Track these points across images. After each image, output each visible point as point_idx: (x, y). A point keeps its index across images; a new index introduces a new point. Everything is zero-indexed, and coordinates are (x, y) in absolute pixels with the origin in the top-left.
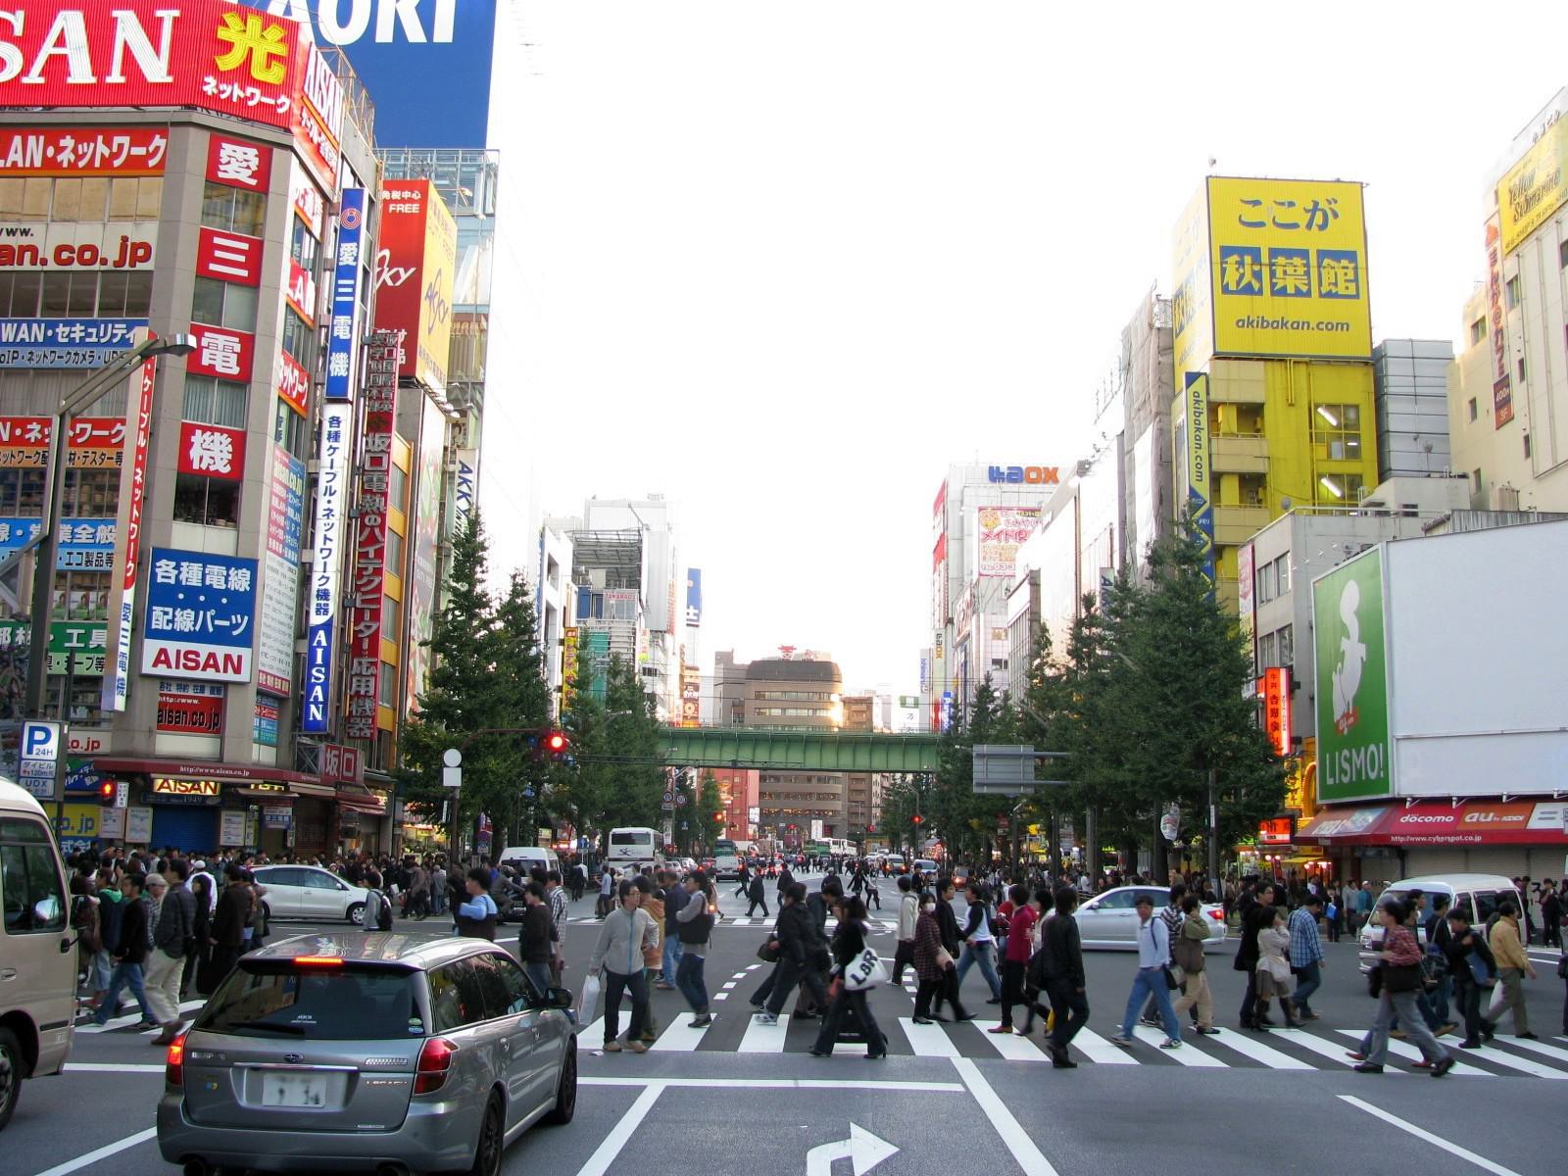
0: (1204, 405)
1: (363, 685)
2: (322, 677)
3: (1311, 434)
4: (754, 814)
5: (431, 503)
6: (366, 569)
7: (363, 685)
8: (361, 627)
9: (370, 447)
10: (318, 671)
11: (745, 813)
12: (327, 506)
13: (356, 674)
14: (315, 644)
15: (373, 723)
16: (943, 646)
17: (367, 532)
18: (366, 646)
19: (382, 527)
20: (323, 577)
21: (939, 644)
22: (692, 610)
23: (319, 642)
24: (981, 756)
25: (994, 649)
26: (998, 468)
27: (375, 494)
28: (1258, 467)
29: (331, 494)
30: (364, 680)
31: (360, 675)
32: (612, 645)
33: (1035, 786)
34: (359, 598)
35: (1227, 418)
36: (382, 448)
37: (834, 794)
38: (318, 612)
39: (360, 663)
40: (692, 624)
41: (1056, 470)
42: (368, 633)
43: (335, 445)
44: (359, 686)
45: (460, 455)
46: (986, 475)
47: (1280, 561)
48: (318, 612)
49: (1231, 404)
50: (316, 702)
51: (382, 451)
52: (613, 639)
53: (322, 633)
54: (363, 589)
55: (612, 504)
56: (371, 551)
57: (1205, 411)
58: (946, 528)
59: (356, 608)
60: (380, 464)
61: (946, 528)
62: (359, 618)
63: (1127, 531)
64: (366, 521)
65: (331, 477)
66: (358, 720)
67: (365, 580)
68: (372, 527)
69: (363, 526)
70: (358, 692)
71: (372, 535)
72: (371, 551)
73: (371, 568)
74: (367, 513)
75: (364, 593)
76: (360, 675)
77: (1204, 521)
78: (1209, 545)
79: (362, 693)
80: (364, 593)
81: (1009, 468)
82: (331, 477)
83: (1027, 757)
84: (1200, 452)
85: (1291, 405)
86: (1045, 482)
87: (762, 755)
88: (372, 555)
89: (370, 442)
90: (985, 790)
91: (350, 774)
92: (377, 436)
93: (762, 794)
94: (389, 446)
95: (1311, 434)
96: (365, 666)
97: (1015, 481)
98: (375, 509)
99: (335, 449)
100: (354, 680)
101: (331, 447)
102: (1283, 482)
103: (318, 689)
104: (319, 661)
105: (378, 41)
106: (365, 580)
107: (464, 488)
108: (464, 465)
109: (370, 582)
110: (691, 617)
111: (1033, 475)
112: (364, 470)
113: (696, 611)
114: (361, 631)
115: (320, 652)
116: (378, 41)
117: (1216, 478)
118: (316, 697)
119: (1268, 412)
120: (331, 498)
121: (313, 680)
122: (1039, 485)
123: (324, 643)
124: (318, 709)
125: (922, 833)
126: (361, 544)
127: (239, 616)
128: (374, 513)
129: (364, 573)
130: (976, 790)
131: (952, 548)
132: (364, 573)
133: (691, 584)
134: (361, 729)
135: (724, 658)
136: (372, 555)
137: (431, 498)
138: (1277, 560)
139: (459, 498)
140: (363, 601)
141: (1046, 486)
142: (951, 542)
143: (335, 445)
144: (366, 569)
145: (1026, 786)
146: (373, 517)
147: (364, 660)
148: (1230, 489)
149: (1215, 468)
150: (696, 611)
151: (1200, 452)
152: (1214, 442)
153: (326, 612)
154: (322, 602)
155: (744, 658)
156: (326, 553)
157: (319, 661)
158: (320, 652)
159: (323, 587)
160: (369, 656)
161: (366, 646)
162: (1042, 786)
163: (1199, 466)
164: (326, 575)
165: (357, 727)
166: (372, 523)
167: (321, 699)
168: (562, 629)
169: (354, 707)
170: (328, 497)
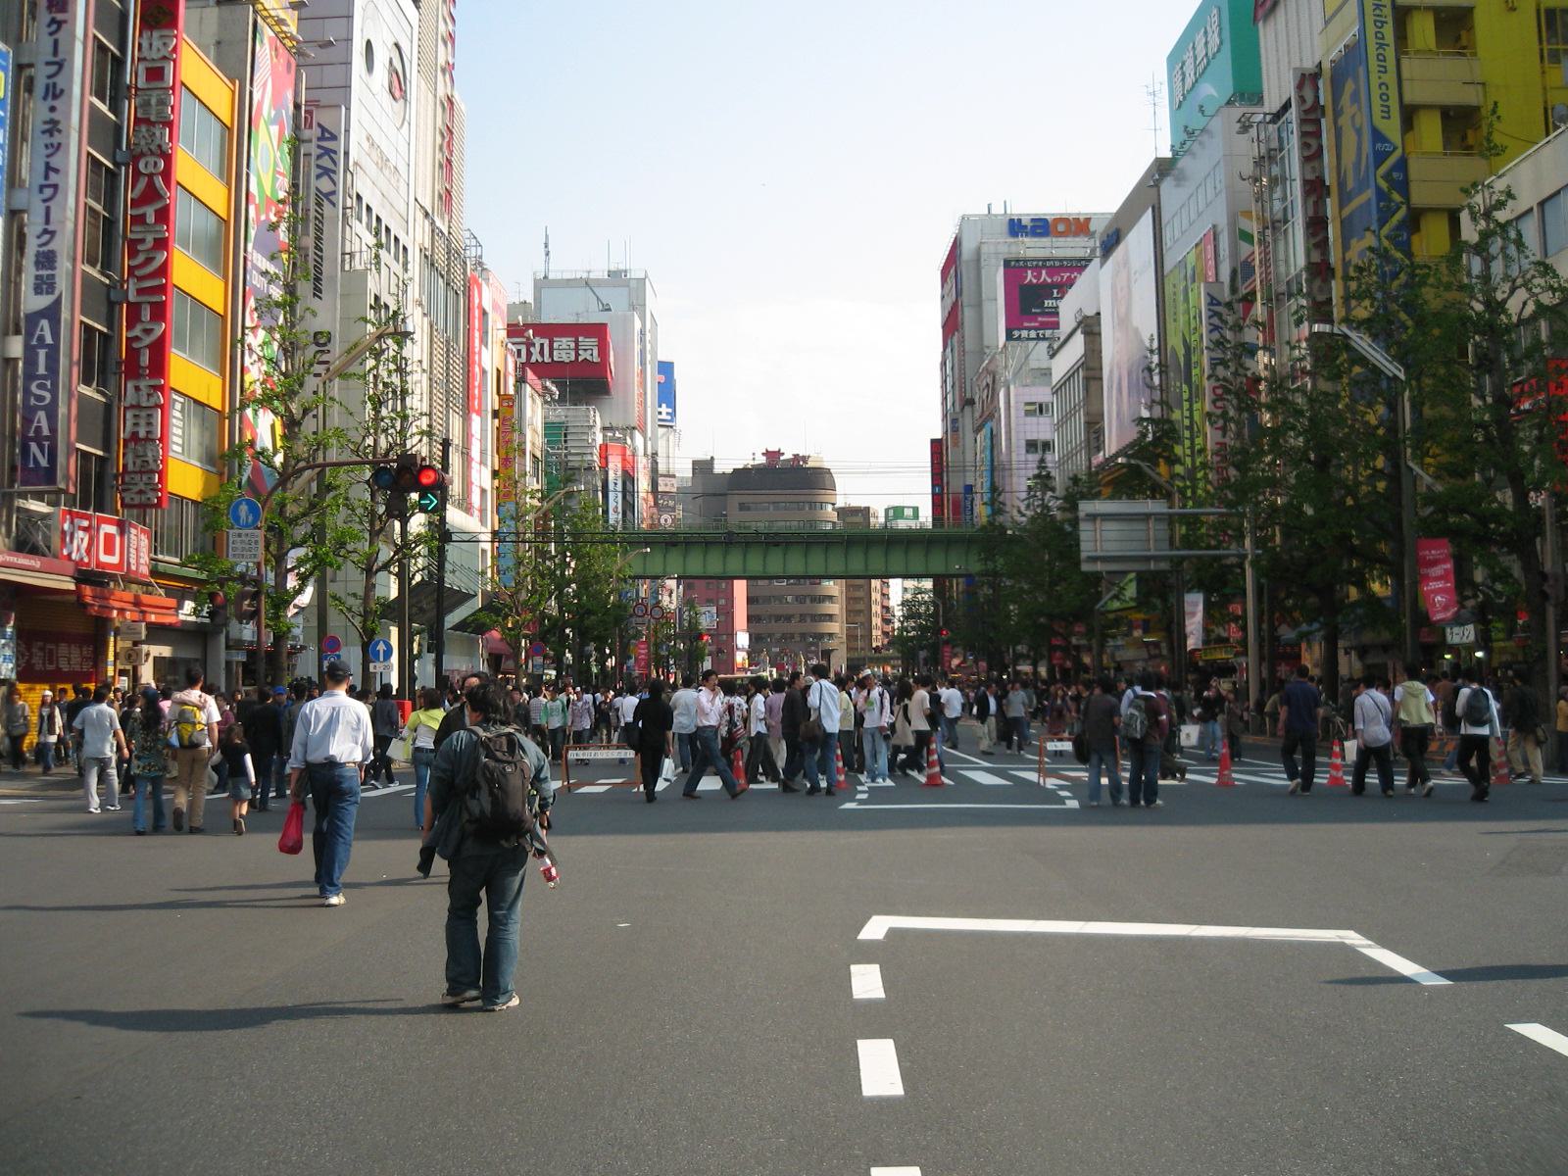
0: (1388, 11)
1: (142, 422)
2: (48, 396)
3: (1542, 50)
4: (742, 639)
5: (274, 180)
6: (142, 241)
7: (142, 422)
8: (137, 331)
9: (146, 53)
10: (41, 387)
11: (732, 635)
12: (48, 116)
13: (132, 407)
14: (34, 342)
15: (161, 480)
16: (960, 433)
17: (142, 183)
18: (145, 359)
19: (167, 175)
20: (45, 231)
21: (955, 430)
22: (664, 409)
23: (41, 338)
24: (1093, 517)
25: (1028, 427)
26: (1020, 220)
27: (153, 124)
28: (1469, 97)
29: (55, 97)
30: (143, 414)
31: (138, 406)
32: (569, 438)
33: (1171, 559)
34: (132, 288)
35: (1423, 30)
36: (164, 53)
37: (831, 616)
38: (38, 290)
39: (137, 389)
40: (668, 425)
41: (1088, 220)
42: (148, 340)
43: (60, 17)
44: (136, 424)
45: (321, 117)
46: (1005, 228)
47: (1547, 206)
48: (38, 290)
49: (1427, 8)
50: (38, 438)
51: (165, 58)
52: (571, 430)
53: (45, 323)
54: (137, 273)
55: (569, 283)
56: (150, 212)
57: (1390, 20)
58: (959, 293)
59: (129, 304)
60: (148, 70)
61: (959, 293)
62: (134, 318)
63: (995, 453)
64: (141, 166)
65: (54, 68)
66: (137, 477)
67: (141, 259)
68: (151, 176)
69: (137, 174)
70: (134, 436)
71: (151, 185)
72: (150, 212)
73: (150, 239)
74: (142, 155)
75: (141, 279)
76: (138, 406)
77: (1395, 175)
78: (1404, 210)
79: (142, 434)
80: (141, 279)
81: (1033, 220)
82: (54, 68)
83: (1158, 517)
84: (1385, 78)
85: (1513, 9)
86: (1076, 234)
87: (755, 564)
88: (151, 219)
89: (145, 44)
90: (1099, 567)
91: (114, 560)
92: (156, 34)
93: (749, 619)
94: (175, 50)
95: (1542, 50)
96: (144, 391)
97: (1041, 235)
98: (153, 147)
99: (60, 24)
100: (129, 415)
101: (53, 21)
102: (1515, 108)
103: (42, 415)
104: (42, 370)
105: (860, 1043)
106: (141, 259)
107: (326, 162)
108: (323, 129)
109: (149, 260)
110: (664, 416)
111: (1061, 228)
112: (137, 89)
113: (670, 410)
114: (137, 339)
115: (42, 353)
116: (860, 1043)
117: (1409, 115)
118: (38, 429)
119: (1480, 19)
120: (55, 103)
121: (33, 401)
122: (1069, 239)
123: (49, 340)
124: (41, 448)
125: (947, 650)
126: (135, 203)
127: (859, 788)
128: (152, 153)
129: (140, 247)
130: (1085, 567)
131: (968, 315)
132: (140, 247)
133: (662, 379)
134: (141, 492)
135: (703, 468)
136: (151, 219)
137: (276, 172)
138: (1542, 204)
139: (318, 177)
140: (140, 292)
141: (1077, 239)
142: (966, 310)
143: (60, 17)
144: (142, 241)
145: (1156, 558)
146: (151, 160)
147: (144, 384)
148: (1430, 130)
149: (1408, 99)
150: (670, 410)
151: (1385, 78)
152: (1405, 62)
153: (51, 289)
154: (45, 273)
155: (723, 466)
156: (48, 192)
157: (42, 370)
158: (42, 353)
159: (45, 249)
160: (152, 376)
161: (145, 359)
162: (1183, 558)
163: (1385, 98)
164: (50, 228)
165: (136, 489)
166: (151, 169)
167: (46, 432)
168: (496, 398)
169: (130, 457)
170: (50, 102)
